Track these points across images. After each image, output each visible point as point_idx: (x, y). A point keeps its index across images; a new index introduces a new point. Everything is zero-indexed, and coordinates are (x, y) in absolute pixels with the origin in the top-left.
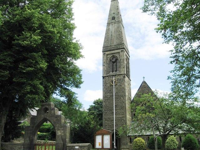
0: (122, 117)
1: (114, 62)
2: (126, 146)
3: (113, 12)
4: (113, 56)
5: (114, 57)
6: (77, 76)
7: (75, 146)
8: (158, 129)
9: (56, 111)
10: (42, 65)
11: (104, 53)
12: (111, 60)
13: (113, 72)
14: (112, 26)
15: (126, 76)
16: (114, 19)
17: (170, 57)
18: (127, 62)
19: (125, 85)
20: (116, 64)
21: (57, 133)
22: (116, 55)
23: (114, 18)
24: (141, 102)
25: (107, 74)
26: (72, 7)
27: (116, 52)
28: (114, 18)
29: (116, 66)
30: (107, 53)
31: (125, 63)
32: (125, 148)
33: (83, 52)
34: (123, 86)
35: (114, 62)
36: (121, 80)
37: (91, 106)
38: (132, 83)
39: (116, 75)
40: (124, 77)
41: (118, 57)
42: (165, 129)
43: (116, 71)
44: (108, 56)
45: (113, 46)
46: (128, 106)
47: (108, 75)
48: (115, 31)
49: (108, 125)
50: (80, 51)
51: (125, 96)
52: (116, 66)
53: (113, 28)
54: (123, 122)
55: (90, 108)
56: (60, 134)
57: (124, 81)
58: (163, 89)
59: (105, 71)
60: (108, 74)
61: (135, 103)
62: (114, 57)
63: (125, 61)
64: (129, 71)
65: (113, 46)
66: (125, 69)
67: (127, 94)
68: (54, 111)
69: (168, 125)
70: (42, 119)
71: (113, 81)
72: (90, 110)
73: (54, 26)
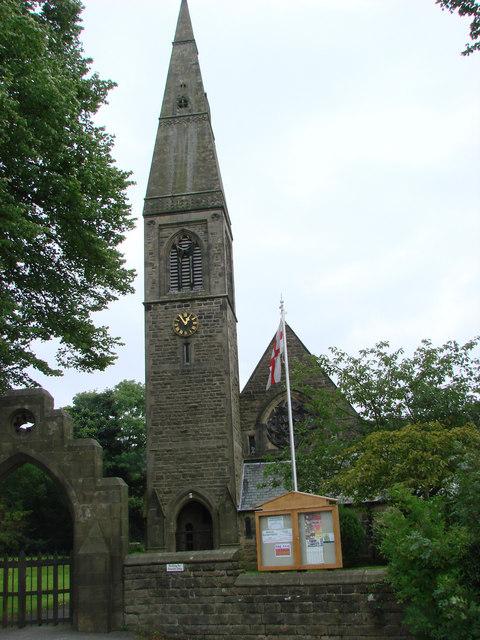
1: (186, 254)
4: (183, 230)
12: (174, 247)
16: (186, 106)
20: (193, 260)
23: (183, 103)
28: (185, 101)
30: (160, 220)
35: (186, 254)
36: (210, 317)
39: (192, 300)
41: (201, 238)
43: (192, 285)
44: (165, 232)
45: (184, 198)
47: (166, 298)
62: (184, 234)
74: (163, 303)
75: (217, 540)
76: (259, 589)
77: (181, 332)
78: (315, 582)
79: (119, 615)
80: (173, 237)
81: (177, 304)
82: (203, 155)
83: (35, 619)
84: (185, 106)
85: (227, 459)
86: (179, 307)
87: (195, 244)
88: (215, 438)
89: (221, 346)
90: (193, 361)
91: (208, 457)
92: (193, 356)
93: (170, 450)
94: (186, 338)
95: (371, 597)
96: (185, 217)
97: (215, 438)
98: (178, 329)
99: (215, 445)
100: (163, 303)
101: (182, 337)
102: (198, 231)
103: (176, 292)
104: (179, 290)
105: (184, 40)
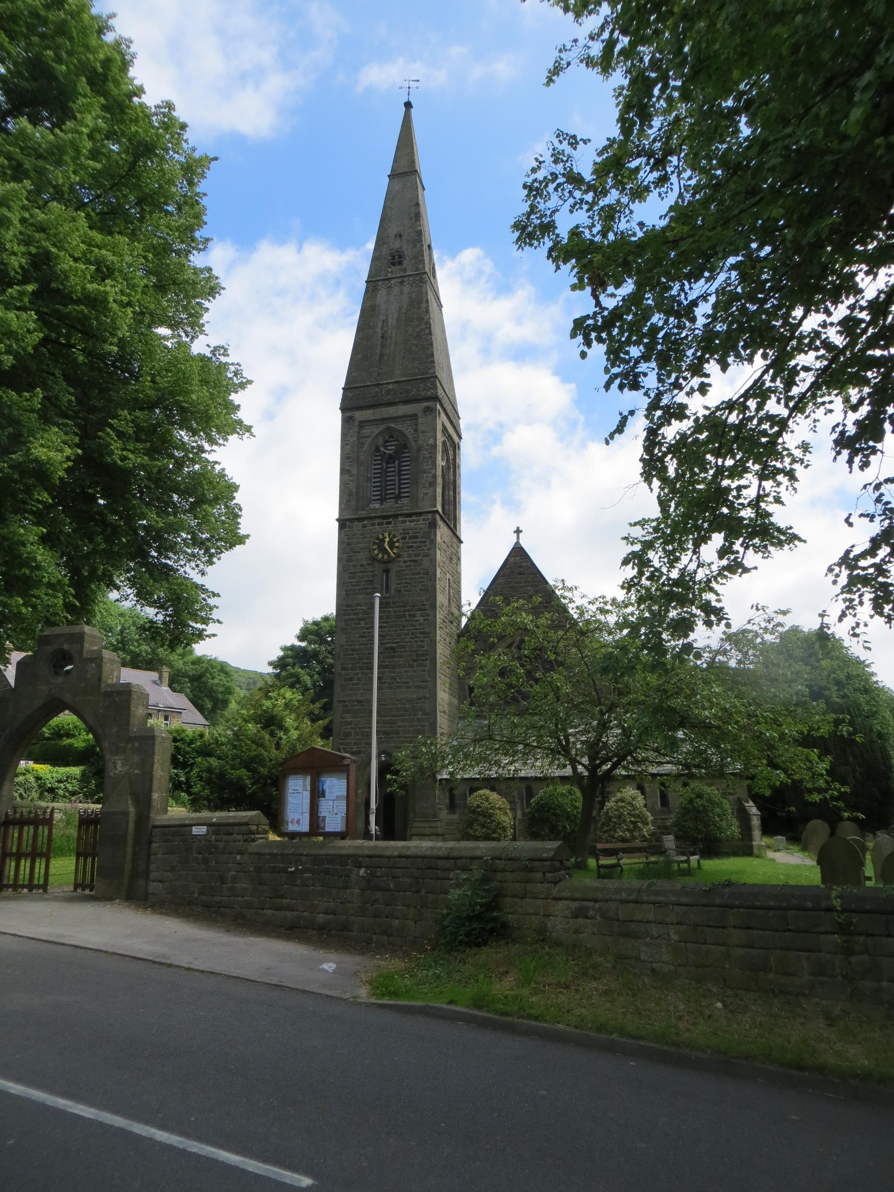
0: (419, 699)
1: (390, 459)
2: (428, 825)
3: (393, 230)
4: (389, 429)
5: (390, 435)
6: (219, 510)
7: (191, 825)
8: (564, 750)
9: (106, 668)
10: (39, 452)
11: (349, 414)
12: (377, 449)
13: (382, 500)
14: (388, 294)
15: (440, 523)
16: (400, 263)
17: (607, 443)
18: (448, 460)
19: (433, 561)
20: (400, 466)
21: (110, 766)
22: (399, 427)
23: (397, 259)
24: (501, 638)
25: (357, 509)
26: (202, 187)
27: (400, 414)
28: (400, 257)
29: (400, 475)
30: (360, 415)
31: (440, 462)
32: (428, 831)
33: (248, 404)
34: (426, 563)
35: (390, 459)
36: (416, 537)
37: (284, 649)
38: (465, 550)
39: (395, 516)
40: (433, 525)
41: (410, 437)
42: (594, 749)
43: (398, 497)
44: (366, 431)
45: (391, 387)
46: (442, 652)
47: (363, 513)
48: (398, 320)
49: (357, 734)
50: (233, 397)
51: (434, 607)
52: (400, 475)
53: (391, 305)
54: (419, 720)
55: (281, 659)
56: (126, 768)
57: (433, 542)
58: (593, 580)
59: (350, 494)
60: (363, 509)
61: (477, 636)
62: (390, 435)
63: (439, 457)
64: (455, 498)
65: (391, 387)
66: (439, 491)
67: (441, 598)
68: (100, 667)
69: (613, 737)
70: (42, 702)
71: (383, 540)
72: (280, 664)
73: (104, 272)
74: (360, 520)
75: (412, 815)
76: (268, 857)
77: (380, 556)
78: (316, 852)
79: (141, 882)
80: (377, 436)
81: (376, 521)
82: (418, 329)
83: (26, 883)
84: (571, 271)
85: (427, 714)
86: (379, 524)
87: (403, 447)
88: (416, 687)
89: (427, 574)
90: (393, 592)
91: (406, 710)
92: (393, 586)
93: (361, 701)
94: (386, 562)
95: (362, 871)
96: (390, 411)
97: (416, 687)
98: (376, 552)
99: (414, 696)
100: (360, 520)
101: (382, 562)
102: (407, 430)
103: (377, 506)
104: (381, 504)
105: (405, 172)
